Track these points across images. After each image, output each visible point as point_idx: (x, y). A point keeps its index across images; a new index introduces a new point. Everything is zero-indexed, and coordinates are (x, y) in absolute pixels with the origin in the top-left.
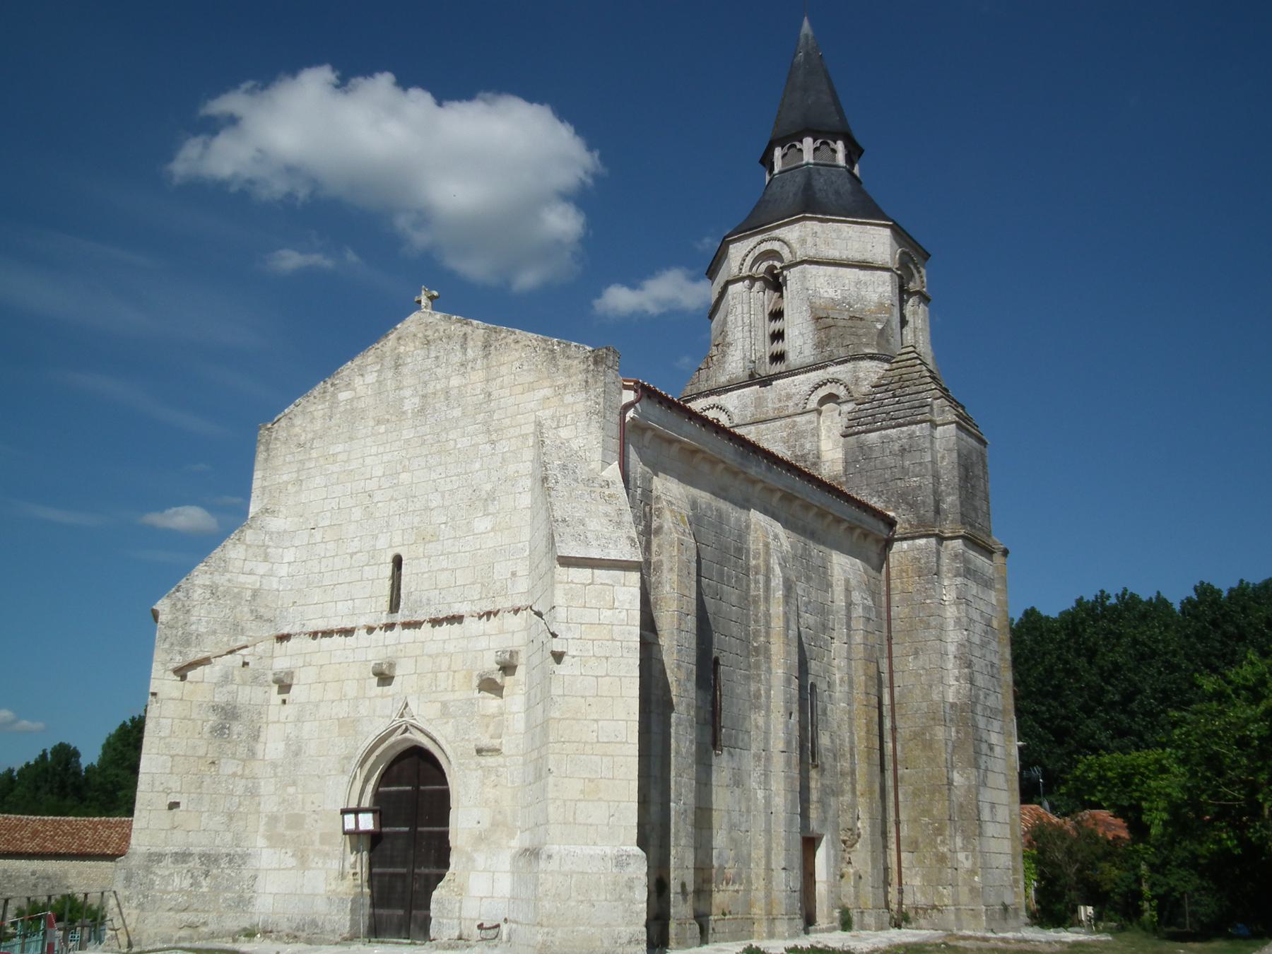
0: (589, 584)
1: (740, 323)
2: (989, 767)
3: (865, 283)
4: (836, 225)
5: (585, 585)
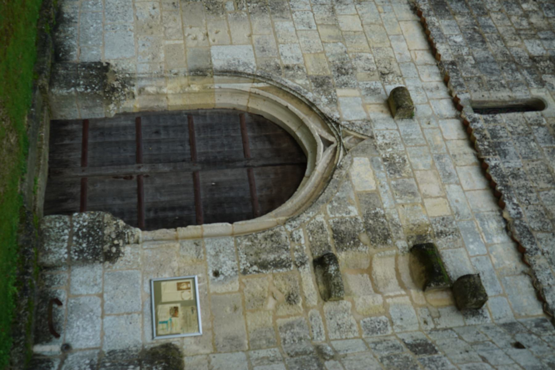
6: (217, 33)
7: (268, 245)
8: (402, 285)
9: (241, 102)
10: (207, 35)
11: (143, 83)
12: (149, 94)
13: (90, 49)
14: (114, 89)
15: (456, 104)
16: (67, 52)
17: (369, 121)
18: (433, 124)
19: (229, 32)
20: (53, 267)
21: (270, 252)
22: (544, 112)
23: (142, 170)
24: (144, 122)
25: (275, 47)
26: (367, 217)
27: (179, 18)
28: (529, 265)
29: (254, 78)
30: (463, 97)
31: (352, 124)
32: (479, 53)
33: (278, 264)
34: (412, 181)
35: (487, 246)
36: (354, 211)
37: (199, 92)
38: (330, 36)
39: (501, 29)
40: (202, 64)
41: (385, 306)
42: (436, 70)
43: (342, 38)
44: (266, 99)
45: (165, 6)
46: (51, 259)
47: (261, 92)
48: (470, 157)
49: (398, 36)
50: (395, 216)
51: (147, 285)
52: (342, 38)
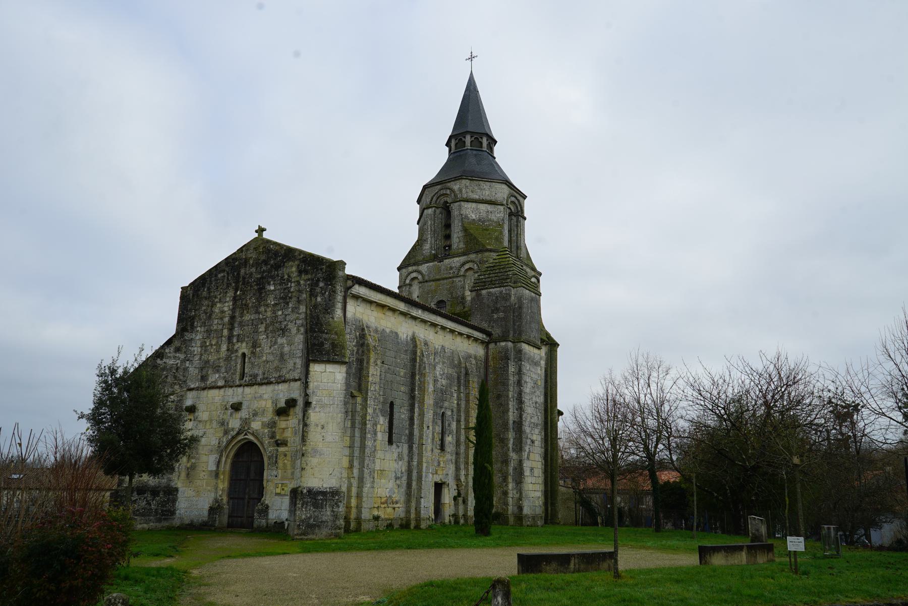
0: (324, 372)
1: (429, 230)
2: (531, 451)
3: (491, 212)
4: (477, 182)
5: (322, 372)
6: (203, 467)
7: (271, 459)
8: (288, 420)
9: (229, 461)
10: (203, 471)
11: (218, 496)
12: (222, 493)
13: (203, 514)
14: (219, 505)
15: (240, 386)
16: (204, 522)
17: (241, 419)
18: (245, 396)
19: (204, 462)
20: (267, 524)
21: (273, 459)
22: (246, 354)
23: (247, 497)
24: (232, 496)
25: (211, 447)
26: (268, 427)
27: (196, 481)
28: (288, 380)
29: (221, 456)
30: (238, 383)
31: (241, 425)
32: (223, 370)
33: (276, 458)
34: (261, 409)
35: (281, 391)
36: (266, 431)
37: (224, 476)
38: (210, 425)
39: (215, 358)
40: (214, 474)
41: (291, 428)
42: (227, 388)
43: (211, 421)
44: (229, 452)
45: (190, 485)
46: (265, 525)
47: (226, 454)
48: (256, 387)
49: (213, 399)
50: (270, 418)
51: (276, 497)
52: (211, 421)
